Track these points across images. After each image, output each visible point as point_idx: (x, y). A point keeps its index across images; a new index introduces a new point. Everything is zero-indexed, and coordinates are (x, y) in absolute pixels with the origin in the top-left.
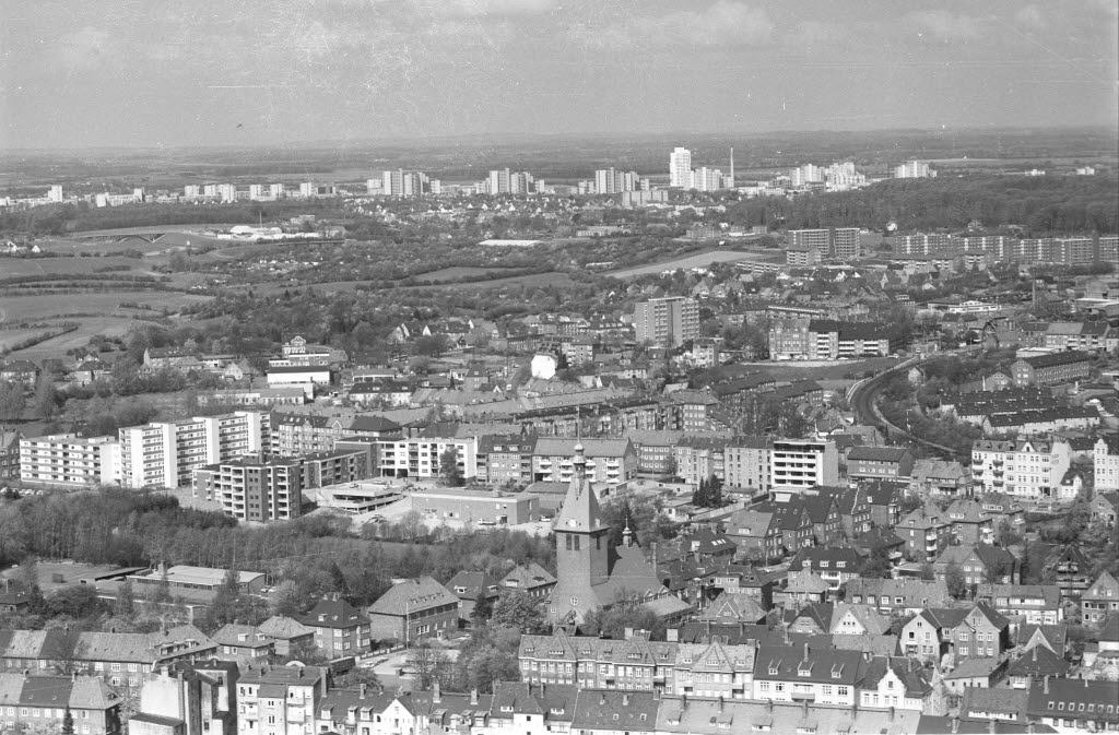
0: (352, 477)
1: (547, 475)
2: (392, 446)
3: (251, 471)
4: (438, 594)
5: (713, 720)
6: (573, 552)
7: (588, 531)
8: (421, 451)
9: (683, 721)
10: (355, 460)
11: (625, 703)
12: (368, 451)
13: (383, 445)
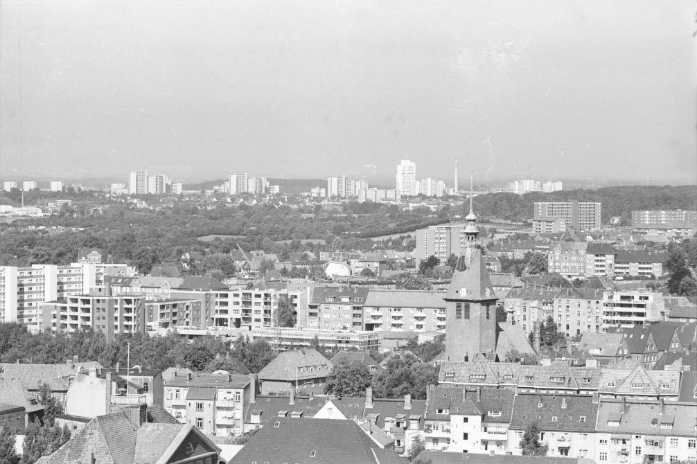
0: (187, 323)
1: (378, 325)
2: (226, 296)
3: (98, 301)
4: (323, 366)
5: (654, 422)
6: (463, 319)
7: (480, 299)
8: (254, 300)
9: (624, 423)
10: (190, 308)
11: (564, 406)
12: (202, 300)
13: (217, 295)
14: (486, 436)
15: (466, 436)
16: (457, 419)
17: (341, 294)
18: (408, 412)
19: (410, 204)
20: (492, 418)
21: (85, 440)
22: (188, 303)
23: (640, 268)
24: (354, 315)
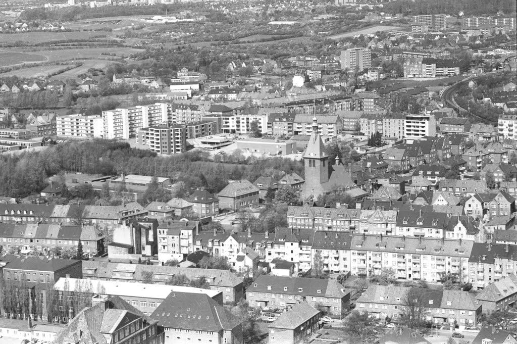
1: (300, 132)
3: (163, 131)
6: (312, 167)
8: (242, 121)
9: (363, 246)
10: (211, 126)
11: (337, 237)
13: (224, 118)
14: (301, 252)
15: (292, 252)
16: (288, 244)
17: (283, 117)
18: (267, 240)
19: (361, 5)
20: (304, 243)
21: (78, 322)
22: (209, 123)
23: (449, 70)
24: (289, 127)
